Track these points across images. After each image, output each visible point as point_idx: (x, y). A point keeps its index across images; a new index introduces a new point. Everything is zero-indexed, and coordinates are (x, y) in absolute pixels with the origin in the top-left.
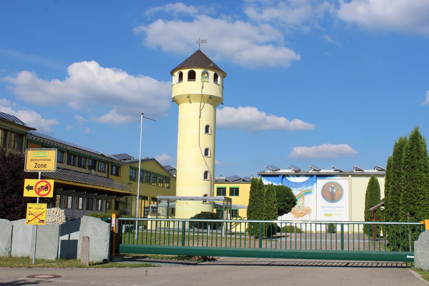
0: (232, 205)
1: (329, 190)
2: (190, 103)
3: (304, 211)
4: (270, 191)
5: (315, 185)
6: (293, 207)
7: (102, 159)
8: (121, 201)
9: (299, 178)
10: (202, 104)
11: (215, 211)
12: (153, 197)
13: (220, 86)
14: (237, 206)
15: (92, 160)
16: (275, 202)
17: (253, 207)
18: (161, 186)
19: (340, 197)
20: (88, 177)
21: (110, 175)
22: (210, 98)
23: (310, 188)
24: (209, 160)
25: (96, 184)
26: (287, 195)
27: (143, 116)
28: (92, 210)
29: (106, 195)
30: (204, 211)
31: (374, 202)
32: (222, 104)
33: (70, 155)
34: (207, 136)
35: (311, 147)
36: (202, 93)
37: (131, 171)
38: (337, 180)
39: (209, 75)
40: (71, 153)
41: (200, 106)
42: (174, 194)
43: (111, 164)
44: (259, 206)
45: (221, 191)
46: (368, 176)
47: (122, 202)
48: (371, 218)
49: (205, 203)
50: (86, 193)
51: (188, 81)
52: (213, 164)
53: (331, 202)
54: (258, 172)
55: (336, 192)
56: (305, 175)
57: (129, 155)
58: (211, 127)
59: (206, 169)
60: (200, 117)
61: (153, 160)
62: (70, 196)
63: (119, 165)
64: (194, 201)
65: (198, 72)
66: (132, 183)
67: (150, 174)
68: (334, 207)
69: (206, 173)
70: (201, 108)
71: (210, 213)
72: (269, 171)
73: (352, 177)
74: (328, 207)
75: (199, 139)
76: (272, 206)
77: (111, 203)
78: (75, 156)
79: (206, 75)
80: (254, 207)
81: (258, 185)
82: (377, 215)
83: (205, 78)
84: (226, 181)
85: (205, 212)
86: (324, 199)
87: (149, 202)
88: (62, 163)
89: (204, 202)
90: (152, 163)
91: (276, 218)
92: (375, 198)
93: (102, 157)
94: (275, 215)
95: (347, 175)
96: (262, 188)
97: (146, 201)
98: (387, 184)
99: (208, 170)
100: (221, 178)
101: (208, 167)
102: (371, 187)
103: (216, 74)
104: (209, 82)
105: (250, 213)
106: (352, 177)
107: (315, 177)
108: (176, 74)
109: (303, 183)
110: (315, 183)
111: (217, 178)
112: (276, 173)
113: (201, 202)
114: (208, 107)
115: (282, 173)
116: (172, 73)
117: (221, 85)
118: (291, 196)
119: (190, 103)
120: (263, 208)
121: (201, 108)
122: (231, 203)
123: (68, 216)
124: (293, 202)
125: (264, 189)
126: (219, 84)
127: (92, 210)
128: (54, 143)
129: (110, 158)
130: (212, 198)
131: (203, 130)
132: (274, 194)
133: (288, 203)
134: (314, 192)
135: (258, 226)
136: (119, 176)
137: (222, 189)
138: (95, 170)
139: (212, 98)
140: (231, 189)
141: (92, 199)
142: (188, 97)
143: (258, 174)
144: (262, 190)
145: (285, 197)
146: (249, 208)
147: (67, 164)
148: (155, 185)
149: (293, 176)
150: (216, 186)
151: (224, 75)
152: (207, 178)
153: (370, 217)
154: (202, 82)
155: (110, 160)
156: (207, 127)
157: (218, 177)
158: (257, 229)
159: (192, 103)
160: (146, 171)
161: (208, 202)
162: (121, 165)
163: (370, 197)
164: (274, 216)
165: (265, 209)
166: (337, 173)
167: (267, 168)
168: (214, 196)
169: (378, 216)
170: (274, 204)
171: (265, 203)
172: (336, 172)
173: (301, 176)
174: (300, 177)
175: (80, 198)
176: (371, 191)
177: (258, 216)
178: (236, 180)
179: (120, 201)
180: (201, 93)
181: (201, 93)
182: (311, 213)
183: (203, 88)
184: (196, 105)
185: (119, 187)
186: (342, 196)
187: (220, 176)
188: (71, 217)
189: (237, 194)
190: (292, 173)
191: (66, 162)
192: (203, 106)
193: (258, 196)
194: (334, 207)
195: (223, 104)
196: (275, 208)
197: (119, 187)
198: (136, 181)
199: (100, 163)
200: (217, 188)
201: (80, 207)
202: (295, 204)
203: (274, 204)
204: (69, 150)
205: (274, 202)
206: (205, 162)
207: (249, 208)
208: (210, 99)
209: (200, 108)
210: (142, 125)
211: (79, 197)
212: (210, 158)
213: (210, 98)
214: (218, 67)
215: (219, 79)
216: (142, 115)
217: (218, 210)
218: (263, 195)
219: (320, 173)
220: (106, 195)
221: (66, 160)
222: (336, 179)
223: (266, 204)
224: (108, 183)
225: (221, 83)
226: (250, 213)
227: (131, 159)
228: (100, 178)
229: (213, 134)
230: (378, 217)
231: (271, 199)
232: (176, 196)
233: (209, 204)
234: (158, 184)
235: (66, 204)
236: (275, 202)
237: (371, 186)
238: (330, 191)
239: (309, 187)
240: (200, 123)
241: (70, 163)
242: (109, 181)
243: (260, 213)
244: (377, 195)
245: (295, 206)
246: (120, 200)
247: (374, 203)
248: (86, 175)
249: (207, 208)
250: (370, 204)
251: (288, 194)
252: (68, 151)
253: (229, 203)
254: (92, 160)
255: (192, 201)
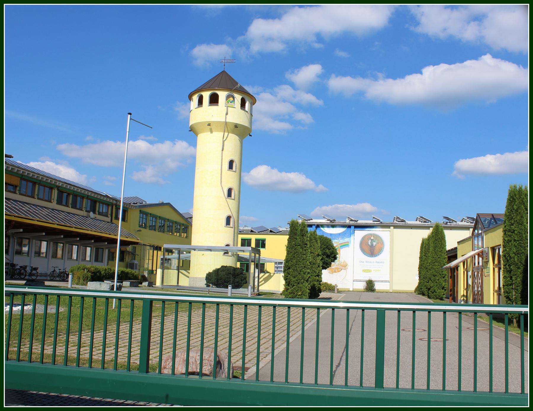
0: (261, 258)
1: (368, 243)
2: (211, 133)
3: (339, 266)
4: (312, 240)
5: (352, 237)
6: (333, 261)
7: (95, 197)
8: (128, 251)
9: (334, 229)
10: (226, 134)
11: (238, 265)
12: (153, 245)
13: (248, 113)
14: (265, 259)
15: (92, 200)
16: (319, 254)
17: (292, 261)
18: (185, 237)
19: (380, 251)
20: (72, 218)
21: (115, 219)
22: (235, 127)
23: (347, 240)
24: (232, 203)
25: (105, 231)
26: (327, 247)
27: (130, 117)
28: (102, 262)
29: (106, 243)
30: (225, 265)
31: (439, 256)
32: (250, 136)
33: (61, 192)
34: (231, 173)
35: (328, 206)
36: (226, 120)
37: (141, 216)
38: (378, 231)
39: (235, 99)
40: (62, 190)
41: (223, 137)
42: (190, 243)
43: (116, 206)
44: (301, 260)
45: (246, 243)
46: (411, 228)
47: (129, 252)
48: (434, 276)
49: (226, 255)
50: (94, 242)
51: (210, 105)
52: (238, 208)
53: (370, 256)
54: (289, 221)
55: (376, 245)
56: (340, 226)
57: (140, 199)
58: (236, 163)
59: (229, 214)
60: (223, 150)
61: (169, 204)
62: (76, 245)
63: (126, 208)
64: (212, 252)
65: (222, 95)
66: (141, 230)
67: (165, 221)
68: (374, 262)
69: (228, 219)
70: (224, 139)
71: (233, 267)
72: (300, 220)
73: (394, 228)
74: (367, 262)
75: (221, 177)
76: (314, 260)
77: (115, 253)
78: (69, 194)
79: (231, 99)
80: (294, 261)
81: (299, 230)
82: (442, 272)
83: (231, 102)
84: (252, 231)
85: (226, 267)
86: (362, 253)
87: (162, 253)
88: (50, 202)
89: (225, 253)
90: (167, 208)
91: (320, 275)
92: (440, 252)
93: (109, 200)
94: (319, 272)
95: (388, 226)
96: (306, 234)
97: (158, 252)
98: (508, 228)
99: (231, 214)
100: (246, 228)
101: (231, 211)
102: (435, 238)
103: (244, 98)
104: (235, 108)
105: (288, 269)
106: (394, 228)
107: (353, 228)
108: (195, 98)
109: (340, 234)
110: (353, 234)
111: (241, 228)
112: (309, 222)
113: (222, 253)
114: (233, 139)
115: (315, 222)
116: (190, 97)
117: (249, 112)
118: (332, 248)
119: (211, 133)
120: (306, 262)
121: (224, 139)
122: (260, 255)
123: (55, 268)
124: (333, 255)
125: (308, 236)
126: (247, 110)
127: (102, 262)
128: (38, 175)
129: (113, 199)
130: (235, 248)
131: (226, 165)
132: (318, 244)
133: (328, 256)
134: (351, 245)
135: (299, 287)
136: (126, 221)
137: (246, 241)
138: (94, 212)
139: (238, 127)
140: (257, 241)
141: (103, 249)
142: (209, 125)
143: (288, 224)
144: (305, 238)
145: (324, 249)
146: (287, 262)
147: (57, 204)
148: (178, 235)
149: (328, 226)
150: (241, 237)
151: (253, 101)
152: (229, 224)
153: (433, 275)
154: (226, 107)
155: (114, 202)
156: (231, 163)
157: (243, 228)
158: (298, 291)
159: (213, 133)
160: (160, 217)
161: (230, 254)
162: (128, 209)
163: (434, 250)
164: (318, 274)
165: (309, 264)
166: (378, 223)
167: (299, 217)
168: (238, 246)
169: (443, 274)
170: (318, 257)
171: (308, 255)
172: (377, 223)
173: (337, 227)
174: (336, 228)
175: (74, 246)
176: (435, 242)
177: (299, 274)
178: (262, 231)
179: (126, 251)
180: (224, 121)
181: (224, 121)
182: (348, 268)
183: (227, 114)
184: (218, 135)
185: (126, 234)
186: (383, 250)
187: (245, 226)
188: (60, 270)
189: (263, 246)
190: (327, 223)
191: (55, 202)
192: (226, 137)
193: (299, 246)
194: (374, 262)
195: (251, 136)
196: (319, 262)
197: (126, 234)
198: (147, 228)
199: (101, 205)
200: (242, 239)
201: (88, 259)
202: (335, 258)
203: (318, 257)
204: (59, 187)
205: (317, 254)
206: (228, 205)
207: (287, 262)
208: (236, 128)
209: (223, 138)
210: (128, 131)
211: (86, 247)
212: (234, 200)
213: (235, 127)
214: (246, 91)
215: (247, 105)
216: (129, 115)
217: (241, 263)
218: (306, 244)
219: (358, 223)
220: (106, 243)
221: (56, 198)
222: (376, 231)
223: (310, 257)
224: (92, 225)
225: (249, 110)
226: (288, 269)
227: (143, 203)
228: (107, 224)
229: (238, 171)
230: (443, 275)
231: (313, 250)
232: (192, 245)
233: (231, 256)
234: (181, 234)
235: (70, 254)
236: (318, 255)
237: (435, 236)
238: (370, 244)
239: (346, 239)
240: (222, 156)
241: (76, 206)
242: (115, 227)
243: (301, 270)
244: (442, 248)
245: (336, 261)
246: (126, 250)
247: (439, 258)
248: (66, 214)
249: (229, 261)
250: (433, 258)
251: (328, 246)
252: (58, 187)
253: (257, 255)
254: (92, 200)
255: (209, 252)
